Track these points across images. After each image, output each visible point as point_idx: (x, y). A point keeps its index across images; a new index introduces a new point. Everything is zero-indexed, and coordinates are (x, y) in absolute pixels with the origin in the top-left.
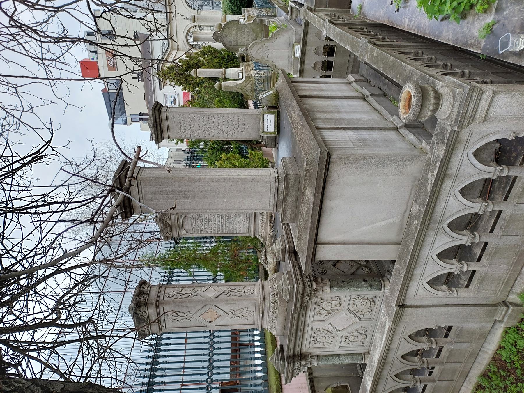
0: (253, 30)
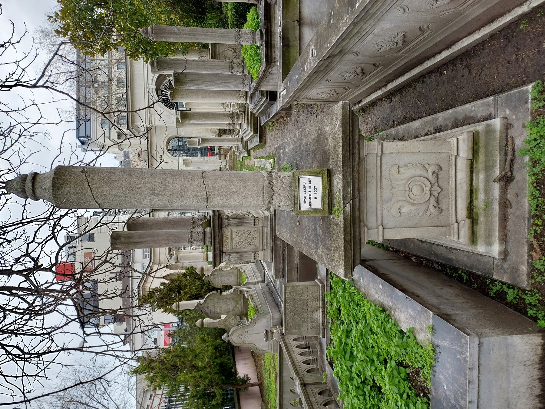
0: (233, 299)
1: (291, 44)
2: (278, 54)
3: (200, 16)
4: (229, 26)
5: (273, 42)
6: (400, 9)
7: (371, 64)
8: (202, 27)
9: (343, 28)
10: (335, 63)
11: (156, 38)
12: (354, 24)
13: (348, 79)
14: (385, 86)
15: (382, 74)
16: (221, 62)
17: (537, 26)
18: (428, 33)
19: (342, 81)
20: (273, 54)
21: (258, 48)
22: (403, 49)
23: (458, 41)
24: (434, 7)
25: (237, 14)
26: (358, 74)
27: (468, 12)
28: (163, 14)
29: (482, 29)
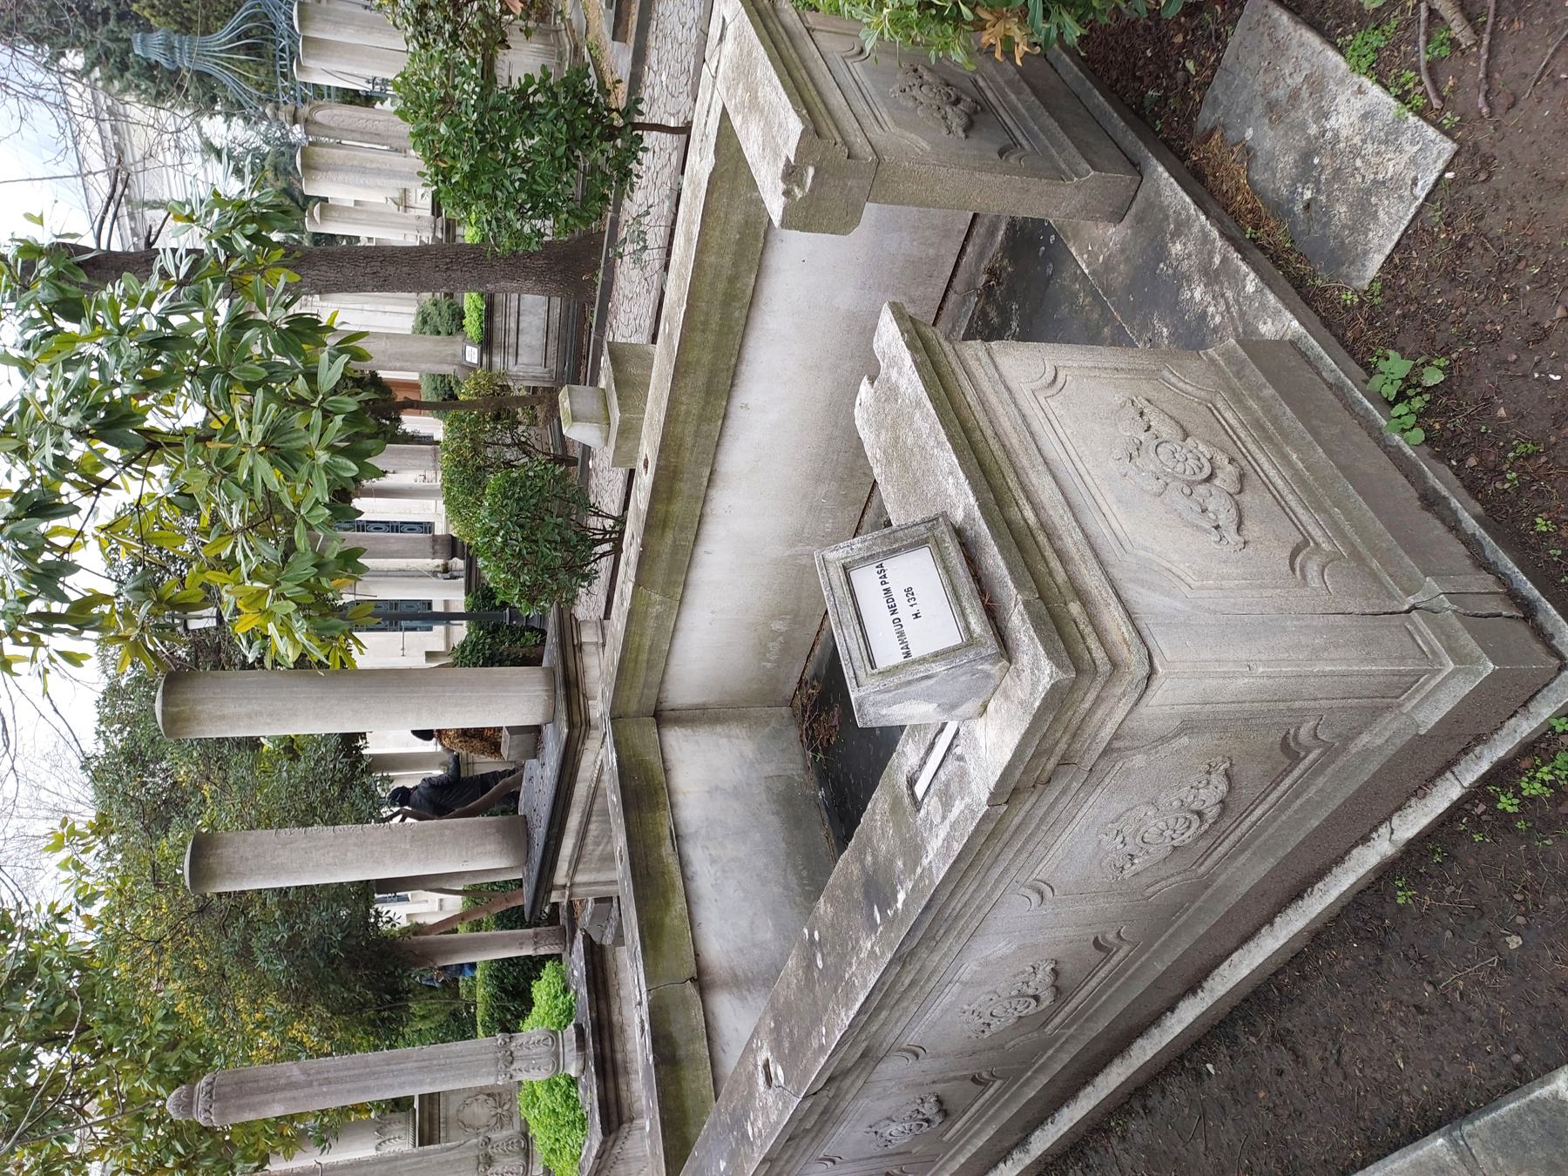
1: (682, 1053)
2: (641, 1090)
3: (386, 1014)
4: (480, 1029)
5: (619, 1056)
6: (1028, 892)
7: (965, 1077)
8: (390, 1047)
9: (865, 978)
10: (849, 1097)
11: (222, 1114)
12: (902, 958)
13: (900, 1142)
14: (1022, 1143)
15: (1005, 1106)
16: (449, 1149)
17: (1448, 890)
18: (1121, 954)
19: (879, 1151)
20: (624, 1094)
21: (573, 1082)
22: (1056, 1013)
23: (1217, 966)
24: (1127, 874)
25: (503, 990)
26: (928, 1121)
27: (1223, 877)
28: (267, 1028)
29: (1277, 920)
